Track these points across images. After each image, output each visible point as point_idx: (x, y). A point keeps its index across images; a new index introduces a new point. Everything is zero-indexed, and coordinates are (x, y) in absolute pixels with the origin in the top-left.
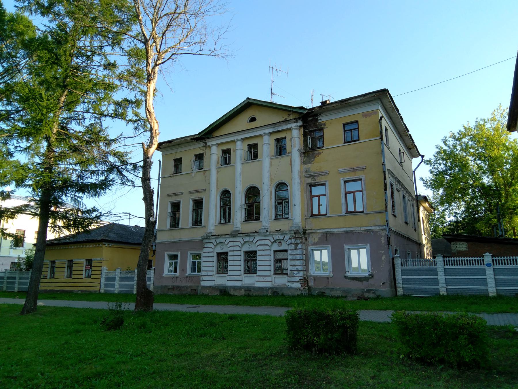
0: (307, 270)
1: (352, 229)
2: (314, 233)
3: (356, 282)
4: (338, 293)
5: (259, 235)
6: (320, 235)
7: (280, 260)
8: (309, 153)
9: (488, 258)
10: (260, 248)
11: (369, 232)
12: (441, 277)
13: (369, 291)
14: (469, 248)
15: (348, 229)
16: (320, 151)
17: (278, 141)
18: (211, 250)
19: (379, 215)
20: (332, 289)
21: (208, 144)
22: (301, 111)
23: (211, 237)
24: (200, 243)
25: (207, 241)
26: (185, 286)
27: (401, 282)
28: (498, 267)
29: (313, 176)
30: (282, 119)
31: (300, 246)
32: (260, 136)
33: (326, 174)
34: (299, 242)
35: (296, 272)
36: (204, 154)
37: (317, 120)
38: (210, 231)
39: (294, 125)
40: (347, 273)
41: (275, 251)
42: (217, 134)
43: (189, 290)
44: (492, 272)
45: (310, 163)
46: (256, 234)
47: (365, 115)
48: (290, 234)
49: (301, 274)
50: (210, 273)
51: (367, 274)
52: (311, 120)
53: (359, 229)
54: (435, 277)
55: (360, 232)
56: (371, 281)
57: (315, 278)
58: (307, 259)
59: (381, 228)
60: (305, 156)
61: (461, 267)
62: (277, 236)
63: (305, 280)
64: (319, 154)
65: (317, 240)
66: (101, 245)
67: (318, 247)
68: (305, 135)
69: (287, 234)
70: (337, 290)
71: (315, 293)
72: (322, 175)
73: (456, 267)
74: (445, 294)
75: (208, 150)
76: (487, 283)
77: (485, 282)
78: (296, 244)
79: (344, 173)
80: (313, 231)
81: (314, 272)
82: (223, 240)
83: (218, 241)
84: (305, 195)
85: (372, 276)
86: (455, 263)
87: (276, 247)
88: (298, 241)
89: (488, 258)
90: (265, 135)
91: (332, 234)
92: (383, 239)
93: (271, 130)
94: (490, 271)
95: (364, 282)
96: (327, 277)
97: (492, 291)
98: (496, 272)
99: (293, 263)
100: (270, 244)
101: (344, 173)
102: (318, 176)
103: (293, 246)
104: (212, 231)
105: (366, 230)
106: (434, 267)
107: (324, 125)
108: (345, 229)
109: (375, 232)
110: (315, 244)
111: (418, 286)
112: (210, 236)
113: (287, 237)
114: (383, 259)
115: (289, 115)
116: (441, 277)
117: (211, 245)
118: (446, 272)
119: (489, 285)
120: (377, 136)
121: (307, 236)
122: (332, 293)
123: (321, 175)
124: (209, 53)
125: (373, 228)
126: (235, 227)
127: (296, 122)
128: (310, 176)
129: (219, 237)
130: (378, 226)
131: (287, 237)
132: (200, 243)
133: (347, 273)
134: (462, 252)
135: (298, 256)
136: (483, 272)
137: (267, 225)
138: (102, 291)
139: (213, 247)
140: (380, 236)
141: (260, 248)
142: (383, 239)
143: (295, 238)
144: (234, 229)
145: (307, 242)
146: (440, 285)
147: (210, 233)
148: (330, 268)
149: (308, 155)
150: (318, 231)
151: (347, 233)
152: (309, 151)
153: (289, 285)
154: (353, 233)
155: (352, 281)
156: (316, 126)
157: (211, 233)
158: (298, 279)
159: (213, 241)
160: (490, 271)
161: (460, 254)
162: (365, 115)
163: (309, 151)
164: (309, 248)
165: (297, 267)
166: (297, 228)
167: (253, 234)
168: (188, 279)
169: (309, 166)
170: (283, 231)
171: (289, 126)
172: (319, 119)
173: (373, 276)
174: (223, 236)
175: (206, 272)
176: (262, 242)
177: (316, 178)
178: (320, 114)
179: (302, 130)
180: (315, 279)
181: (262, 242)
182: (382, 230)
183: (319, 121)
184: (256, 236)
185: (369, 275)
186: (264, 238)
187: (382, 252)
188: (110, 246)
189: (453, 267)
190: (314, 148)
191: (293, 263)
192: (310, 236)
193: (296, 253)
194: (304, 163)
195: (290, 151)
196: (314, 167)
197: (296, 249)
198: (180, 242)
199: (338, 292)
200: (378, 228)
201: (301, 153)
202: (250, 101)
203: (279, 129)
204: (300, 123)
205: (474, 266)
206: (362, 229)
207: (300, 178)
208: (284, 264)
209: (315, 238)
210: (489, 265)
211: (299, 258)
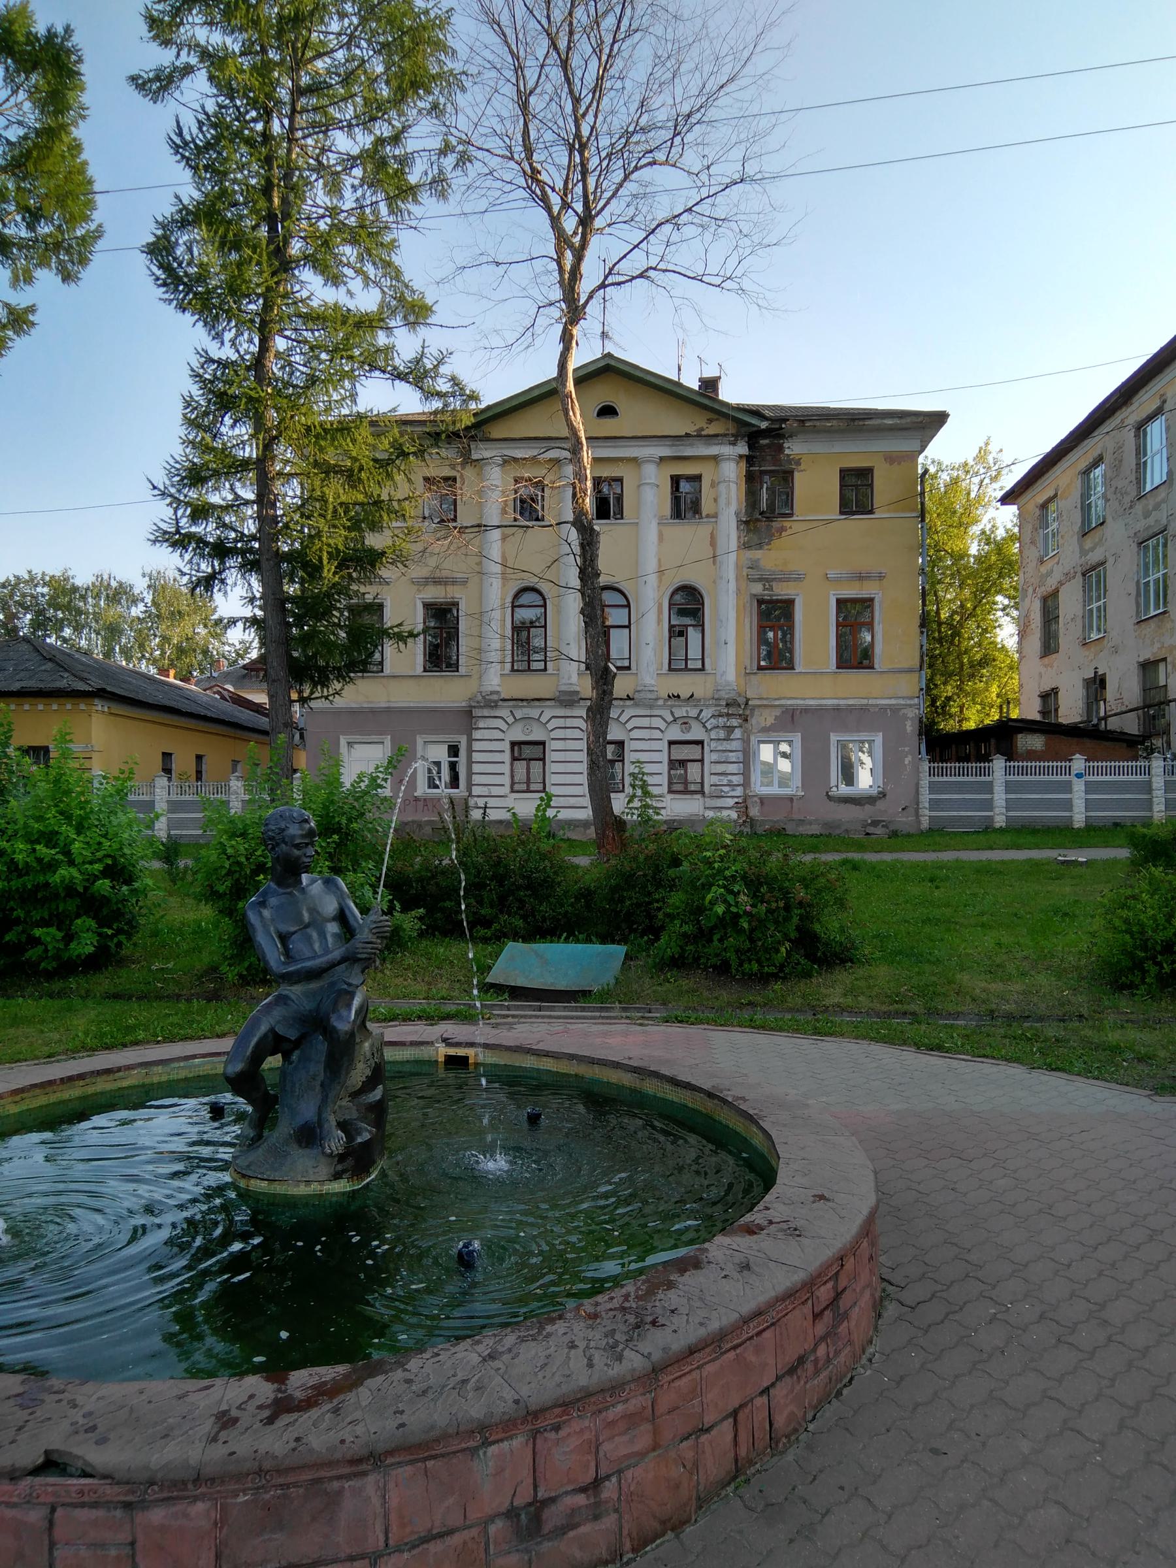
0: (746, 784)
1: (851, 702)
2: (766, 706)
3: (852, 807)
4: (815, 829)
5: (636, 705)
6: (777, 712)
7: (683, 763)
8: (759, 524)
9: (1078, 763)
10: (636, 734)
11: (883, 709)
12: (1000, 797)
13: (875, 823)
14: (1046, 744)
15: (842, 702)
16: (785, 524)
17: (676, 480)
18: (497, 734)
19: (905, 677)
20: (801, 822)
21: (475, 456)
22: (754, 421)
23: (500, 703)
24: (467, 718)
25: (486, 712)
26: (413, 822)
27: (927, 805)
28: (1091, 778)
29: (767, 580)
30: (691, 430)
31: (737, 733)
32: (634, 460)
33: (799, 579)
34: (735, 724)
35: (726, 789)
36: (458, 480)
37: (780, 449)
38: (491, 689)
39: (726, 450)
40: (834, 789)
41: (671, 743)
42: (497, 431)
43: (428, 830)
44: (1083, 788)
45: (760, 546)
46: (628, 703)
47: (891, 459)
48: (716, 705)
49: (739, 791)
50: (496, 791)
51: (874, 792)
52: (768, 446)
53: (865, 702)
54: (1068, 796)
55: (864, 709)
56: (880, 805)
57: (763, 800)
58: (747, 757)
59: (909, 702)
60: (749, 531)
61: (1033, 778)
62: (684, 709)
63: (743, 806)
64: (782, 529)
65: (770, 721)
66: (82, 707)
67: (774, 736)
68: (751, 479)
69: (708, 706)
70: (811, 824)
71: (760, 830)
72: (788, 580)
73: (1025, 778)
74: (1083, 825)
75: (469, 473)
76: (1072, 806)
77: (1068, 805)
78: (730, 729)
79: (837, 580)
80: (765, 702)
81: (759, 788)
82: (534, 713)
83: (519, 714)
84: (747, 621)
85: (883, 795)
86: (1023, 771)
87: (675, 733)
88: (734, 722)
89: (1078, 763)
90: (648, 461)
91: (806, 710)
92: (909, 723)
93: (666, 452)
94: (1079, 786)
95: (867, 807)
96: (791, 799)
97: (1079, 818)
98: (1090, 788)
99: (720, 768)
100: (663, 725)
101: (837, 580)
102: (780, 580)
103: (722, 734)
104: (498, 689)
105: (877, 705)
106: (987, 779)
107: (798, 463)
108: (835, 702)
109: (895, 709)
110: (765, 730)
111: (955, 813)
112: (496, 702)
113: (707, 714)
114: (906, 762)
115: (710, 421)
116: (1000, 797)
117: (499, 723)
118: (1009, 787)
119: (1076, 810)
120: (913, 510)
121: (748, 712)
122: (801, 829)
123: (786, 578)
124: (717, 281)
125: (893, 702)
126: (564, 681)
127: (734, 444)
128: (760, 580)
129: (525, 703)
130: (903, 698)
131: (707, 714)
132: (467, 718)
133: (834, 789)
134: (1035, 752)
135: (731, 754)
136: (1067, 787)
137: (653, 682)
138: (925, 823)
139: (504, 727)
140: (905, 718)
141: (636, 734)
142: (909, 723)
143: (728, 715)
144: (563, 688)
145: (748, 725)
146: (997, 811)
147: (492, 693)
148: (797, 781)
149: (755, 527)
150: (777, 703)
151: (837, 709)
152: (758, 520)
153: (710, 814)
154: (850, 709)
155: (842, 805)
156: (776, 461)
157: (497, 693)
158: (730, 802)
159: (504, 713)
160: (1079, 786)
161: (1031, 755)
162: (891, 459)
163: (758, 520)
164: (752, 738)
165: (730, 777)
166: (733, 695)
167: (621, 703)
168: (421, 804)
169: (757, 554)
170: (699, 700)
171: (714, 450)
172: (786, 445)
173: (885, 796)
174: (537, 703)
175: (485, 789)
176: (645, 722)
177: (774, 584)
178: (791, 436)
179: (743, 464)
180: (762, 803)
181: (645, 722)
182: (910, 706)
183: (787, 452)
184: (628, 706)
185: (879, 793)
186: (648, 712)
187: (907, 749)
188: (106, 709)
189: (1020, 778)
190: (770, 514)
191: (720, 768)
192: (756, 712)
193: (729, 748)
194: (746, 546)
195: (712, 512)
196: (770, 558)
197: (727, 739)
198: (388, 711)
199: (813, 827)
200: (902, 702)
201: (740, 522)
202: (613, 363)
203: (688, 452)
204: (742, 449)
205: (1055, 778)
206: (871, 702)
207: (737, 580)
208: (693, 770)
209: (765, 718)
210: (1079, 776)
211: (734, 760)
